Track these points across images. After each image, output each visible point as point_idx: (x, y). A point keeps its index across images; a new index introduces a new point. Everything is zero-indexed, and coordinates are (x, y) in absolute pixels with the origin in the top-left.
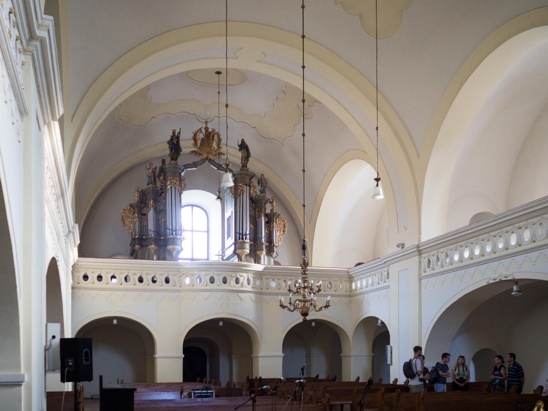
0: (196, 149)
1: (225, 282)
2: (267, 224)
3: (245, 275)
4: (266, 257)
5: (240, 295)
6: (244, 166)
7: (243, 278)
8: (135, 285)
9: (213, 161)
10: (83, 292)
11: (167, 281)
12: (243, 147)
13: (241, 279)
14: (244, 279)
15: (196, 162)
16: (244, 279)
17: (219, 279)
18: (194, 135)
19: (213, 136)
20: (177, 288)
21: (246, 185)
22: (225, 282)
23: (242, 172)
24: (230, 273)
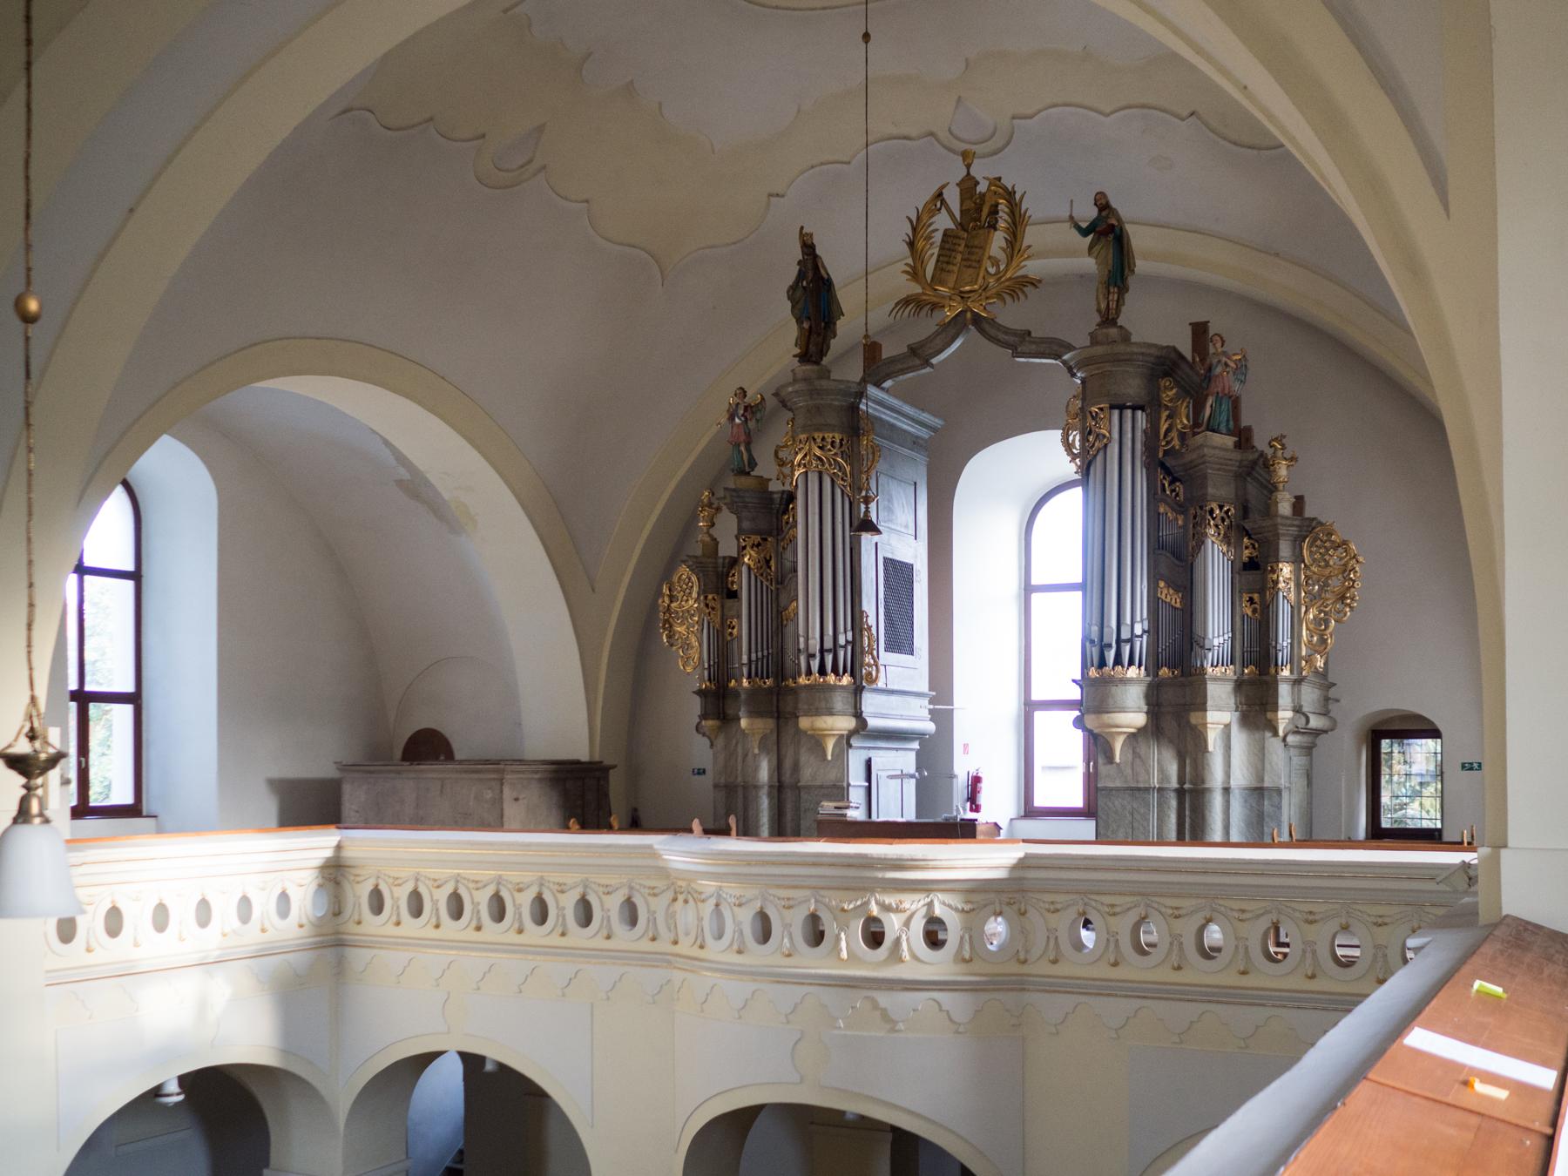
0: (917, 289)
1: (816, 936)
2: (1252, 576)
3: (914, 903)
4: (1239, 739)
5: (884, 999)
6: (1109, 319)
7: (904, 921)
8: (520, 931)
9: (992, 322)
10: (365, 954)
11: (631, 914)
12: (1107, 231)
13: (893, 925)
14: (907, 924)
15: (922, 344)
16: (907, 924)
17: (786, 926)
18: (914, 229)
19: (994, 211)
20: (664, 946)
21: (1122, 408)
22: (816, 936)
23: (1099, 350)
24: (833, 898)
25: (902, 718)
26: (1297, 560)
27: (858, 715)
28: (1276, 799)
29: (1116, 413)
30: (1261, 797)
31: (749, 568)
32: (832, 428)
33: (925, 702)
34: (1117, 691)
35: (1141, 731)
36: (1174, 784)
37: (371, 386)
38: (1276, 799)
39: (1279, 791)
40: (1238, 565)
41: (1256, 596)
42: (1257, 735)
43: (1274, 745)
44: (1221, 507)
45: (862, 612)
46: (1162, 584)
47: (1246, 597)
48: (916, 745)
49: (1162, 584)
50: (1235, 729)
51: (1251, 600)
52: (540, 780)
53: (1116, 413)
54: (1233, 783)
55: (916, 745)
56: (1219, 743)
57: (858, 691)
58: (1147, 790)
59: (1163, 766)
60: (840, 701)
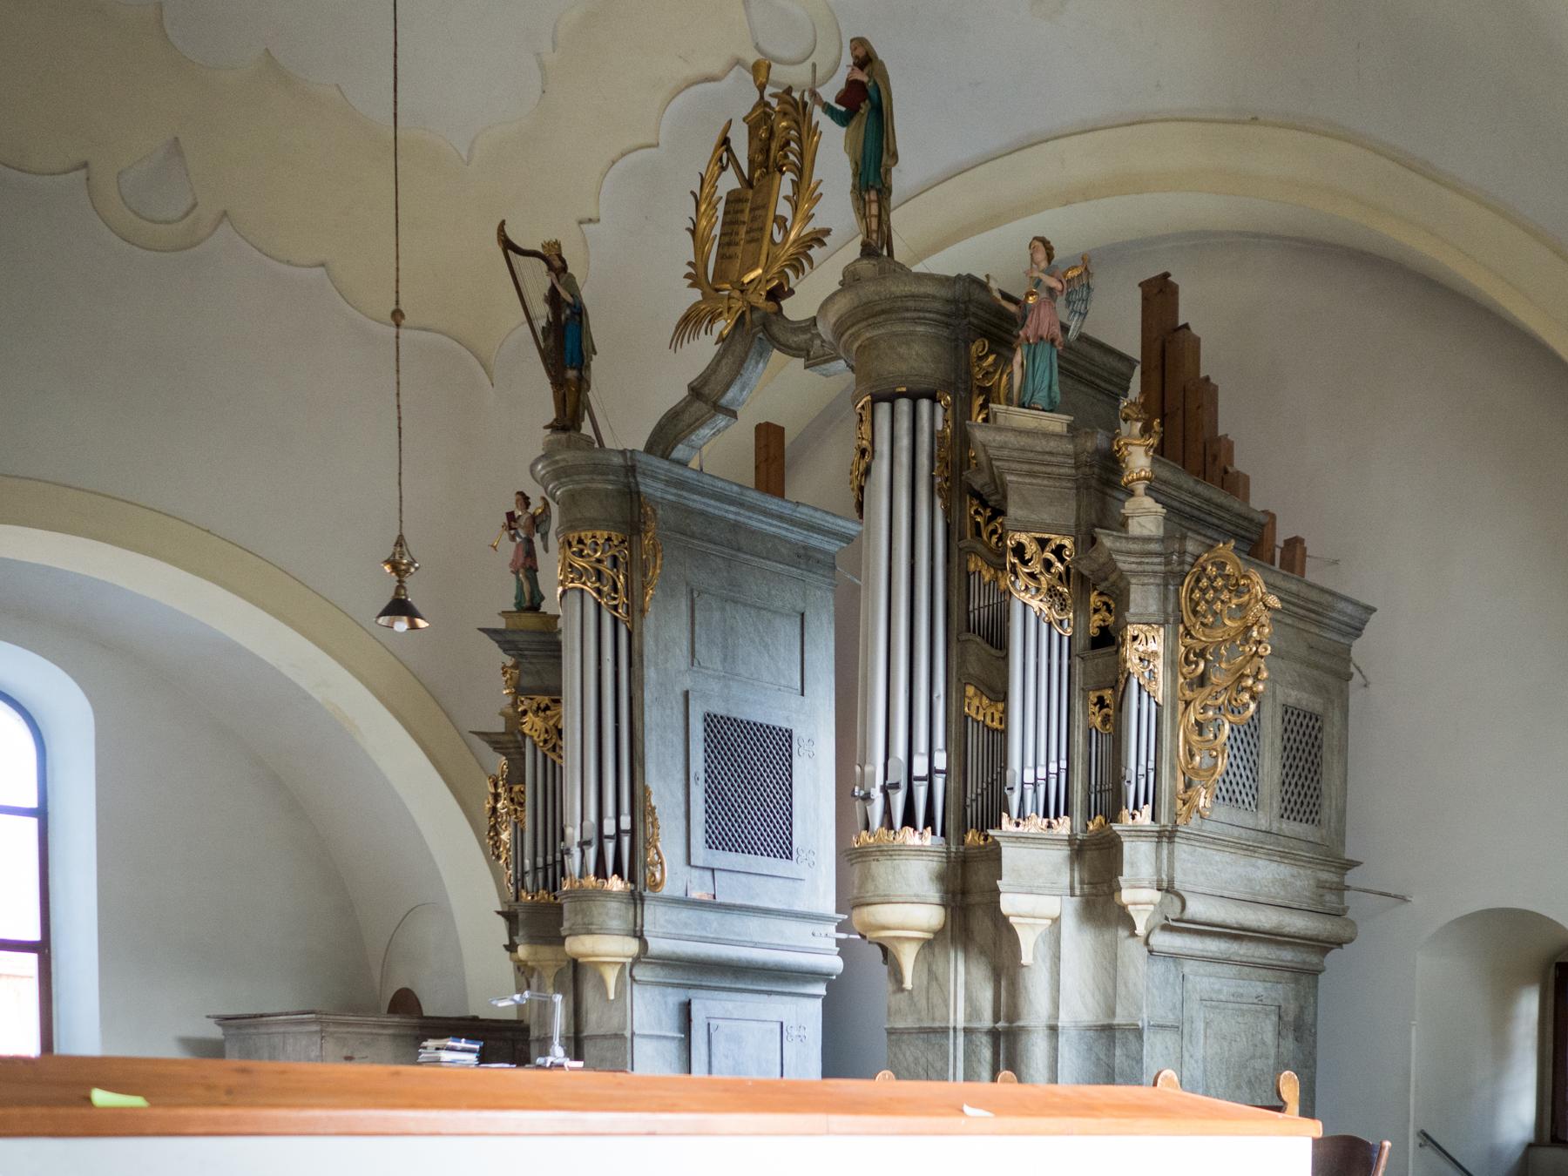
2: (1102, 656)
4: (1078, 944)
15: (705, 378)
21: (892, 398)
25: (755, 945)
26: (1172, 619)
27: (638, 934)
28: (1133, 1046)
29: (904, 405)
30: (1112, 1042)
31: (535, 746)
32: (593, 524)
33: (832, 928)
34: (881, 869)
35: (939, 933)
36: (987, 1022)
37: (109, 547)
38: (1133, 1046)
39: (1138, 1032)
40: (1081, 643)
41: (1108, 694)
42: (1108, 936)
43: (1132, 950)
44: (1043, 543)
45: (646, 789)
46: (970, 690)
47: (1093, 697)
48: (821, 989)
49: (970, 690)
50: (1069, 925)
51: (1101, 702)
52: (394, 1036)
53: (883, 409)
54: (1064, 1020)
55: (821, 989)
56: (1044, 950)
57: (636, 899)
58: (945, 1031)
59: (965, 991)
60: (614, 914)
